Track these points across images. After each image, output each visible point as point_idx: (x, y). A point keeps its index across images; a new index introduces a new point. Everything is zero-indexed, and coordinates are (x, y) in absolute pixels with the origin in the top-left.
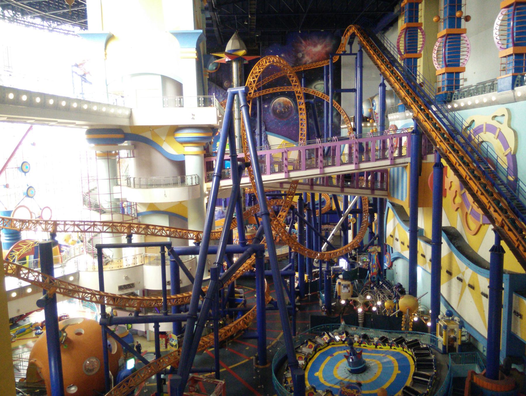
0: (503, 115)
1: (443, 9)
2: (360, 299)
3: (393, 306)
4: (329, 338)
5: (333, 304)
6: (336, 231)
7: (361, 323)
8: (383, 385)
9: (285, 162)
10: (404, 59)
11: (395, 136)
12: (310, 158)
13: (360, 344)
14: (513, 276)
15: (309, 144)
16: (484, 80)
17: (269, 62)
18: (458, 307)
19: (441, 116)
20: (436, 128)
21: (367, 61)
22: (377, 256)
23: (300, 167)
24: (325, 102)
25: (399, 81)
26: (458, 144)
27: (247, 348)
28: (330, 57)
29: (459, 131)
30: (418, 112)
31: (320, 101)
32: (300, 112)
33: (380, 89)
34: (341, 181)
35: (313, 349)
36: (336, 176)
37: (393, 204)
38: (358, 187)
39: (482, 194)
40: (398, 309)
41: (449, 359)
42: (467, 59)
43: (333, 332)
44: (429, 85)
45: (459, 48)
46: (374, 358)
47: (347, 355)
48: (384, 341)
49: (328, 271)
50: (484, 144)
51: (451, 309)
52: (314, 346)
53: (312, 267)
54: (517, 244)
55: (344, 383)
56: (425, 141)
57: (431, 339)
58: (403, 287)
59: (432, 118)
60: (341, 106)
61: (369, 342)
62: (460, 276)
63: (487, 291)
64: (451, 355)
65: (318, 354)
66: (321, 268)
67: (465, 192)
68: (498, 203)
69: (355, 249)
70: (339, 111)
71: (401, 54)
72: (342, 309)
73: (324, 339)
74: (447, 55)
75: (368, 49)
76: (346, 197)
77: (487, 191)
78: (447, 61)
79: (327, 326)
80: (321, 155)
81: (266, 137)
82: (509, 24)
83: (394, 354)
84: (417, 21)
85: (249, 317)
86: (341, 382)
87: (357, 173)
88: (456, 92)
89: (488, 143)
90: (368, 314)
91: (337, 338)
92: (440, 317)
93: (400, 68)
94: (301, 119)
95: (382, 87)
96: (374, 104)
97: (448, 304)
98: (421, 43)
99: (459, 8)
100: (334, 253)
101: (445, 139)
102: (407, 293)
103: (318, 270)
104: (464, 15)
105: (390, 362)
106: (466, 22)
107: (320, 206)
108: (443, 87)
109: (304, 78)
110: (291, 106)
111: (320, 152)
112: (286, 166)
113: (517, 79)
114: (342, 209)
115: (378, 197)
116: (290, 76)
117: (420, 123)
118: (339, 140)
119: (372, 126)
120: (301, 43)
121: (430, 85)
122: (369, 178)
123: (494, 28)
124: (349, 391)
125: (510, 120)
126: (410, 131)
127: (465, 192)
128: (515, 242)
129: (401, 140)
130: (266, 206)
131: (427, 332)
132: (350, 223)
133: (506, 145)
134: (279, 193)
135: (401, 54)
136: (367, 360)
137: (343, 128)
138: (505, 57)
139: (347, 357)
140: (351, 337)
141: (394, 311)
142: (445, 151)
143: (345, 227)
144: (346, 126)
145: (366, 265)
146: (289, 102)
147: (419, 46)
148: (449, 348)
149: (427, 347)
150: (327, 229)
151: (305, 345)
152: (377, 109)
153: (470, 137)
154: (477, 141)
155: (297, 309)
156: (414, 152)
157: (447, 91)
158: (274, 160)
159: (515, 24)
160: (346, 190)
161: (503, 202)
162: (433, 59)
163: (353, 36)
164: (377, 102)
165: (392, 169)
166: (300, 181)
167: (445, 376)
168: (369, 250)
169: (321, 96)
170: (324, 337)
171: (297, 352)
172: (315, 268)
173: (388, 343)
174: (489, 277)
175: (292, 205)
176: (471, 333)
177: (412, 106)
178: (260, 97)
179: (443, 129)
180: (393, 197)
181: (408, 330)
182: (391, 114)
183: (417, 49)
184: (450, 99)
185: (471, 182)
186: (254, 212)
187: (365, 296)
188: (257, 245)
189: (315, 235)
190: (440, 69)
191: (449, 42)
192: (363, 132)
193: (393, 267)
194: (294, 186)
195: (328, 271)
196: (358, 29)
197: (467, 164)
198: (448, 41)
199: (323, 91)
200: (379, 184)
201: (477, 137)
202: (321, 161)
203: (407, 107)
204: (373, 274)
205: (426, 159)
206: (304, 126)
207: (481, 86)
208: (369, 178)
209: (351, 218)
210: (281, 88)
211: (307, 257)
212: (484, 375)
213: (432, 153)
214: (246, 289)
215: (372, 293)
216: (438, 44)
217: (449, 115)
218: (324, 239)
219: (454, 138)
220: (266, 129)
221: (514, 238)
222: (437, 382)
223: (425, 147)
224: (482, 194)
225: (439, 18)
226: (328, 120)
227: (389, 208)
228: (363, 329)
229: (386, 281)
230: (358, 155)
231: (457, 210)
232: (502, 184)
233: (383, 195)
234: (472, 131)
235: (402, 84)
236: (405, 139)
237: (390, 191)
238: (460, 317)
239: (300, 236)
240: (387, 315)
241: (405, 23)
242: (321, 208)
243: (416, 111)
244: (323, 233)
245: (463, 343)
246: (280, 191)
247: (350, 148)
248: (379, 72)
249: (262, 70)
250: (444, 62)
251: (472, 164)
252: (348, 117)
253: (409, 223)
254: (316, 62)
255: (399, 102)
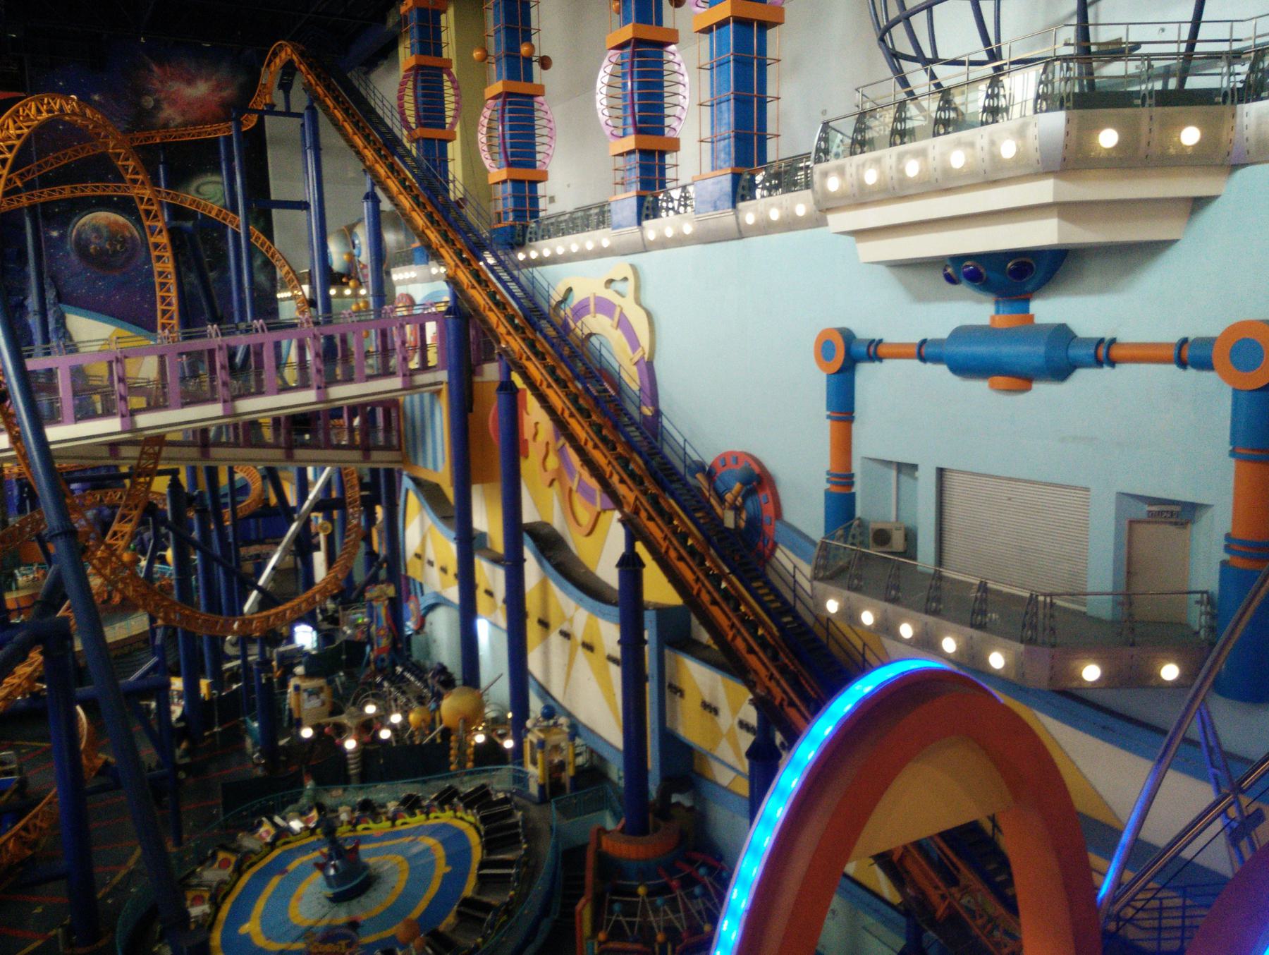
0: (625, 279)
1: (492, 34)
2: (351, 716)
3: (428, 719)
4: (273, 831)
5: (282, 742)
6: (281, 560)
7: (355, 775)
8: (409, 911)
9: (118, 387)
10: (417, 141)
11: (410, 319)
12: (195, 375)
13: (355, 825)
14: (663, 612)
15: (188, 337)
16: (587, 202)
17: (49, 111)
18: (565, 693)
19: (505, 277)
20: (497, 304)
21: (329, 135)
22: (386, 607)
23: (165, 400)
24: (230, 231)
25: (408, 189)
26: (543, 341)
27: (39, 910)
28: (234, 115)
29: (542, 310)
30: (457, 266)
31: (213, 229)
32: (157, 253)
33: (366, 207)
34: (283, 431)
35: (231, 868)
36: (269, 421)
37: (417, 482)
38: (329, 446)
39: (596, 446)
40: (441, 722)
41: (552, 811)
42: (550, 152)
43: (283, 814)
44: (475, 204)
45: (532, 128)
46: (389, 850)
47: (322, 860)
48: (411, 804)
49: (265, 663)
50: (593, 339)
51: (551, 703)
52: (233, 859)
53: (221, 657)
54: (664, 545)
55: (314, 934)
56: (477, 332)
57: (514, 777)
58: (450, 669)
59: (486, 281)
60: (272, 242)
61: (375, 817)
62: (565, 627)
63: (616, 651)
64: (556, 802)
65: (246, 878)
66: (244, 656)
67: (563, 446)
68: (625, 462)
69: (334, 598)
70: (269, 256)
71: (409, 128)
72: (306, 750)
73: (260, 835)
74: (508, 141)
75: (328, 107)
76: (302, 473)
77: (604, 440)
78: (509, 153)
79: (268, 801)
80: (223, 367)
81: (61, 321)
82: (625, 85)
83: (434, 831)
84: (438, 53)
85: (35, 825)
86: (307, 933)
87: (325, 411)
88: (533, 225)
89: (599, 337)
90: (371, 746)
91: (296, 825)
92: (529, 724)
93: (408, 160)
94: (161, 274)
95: (370, 203)
96: (357, 242)
97: (545, 693)
98: (453, 106)
99: (527, 37)
100: (276, 614)
101: (516, 328)
102: (459, 682)
103: (238, 662)
104: (537, 54)
105: (428, 851)
106: (543, 71)
107: (233, 499)
108: (506, 213)
109: (164, 163)
110: (132, 237)
111: (220, 359)
112: (123, 398)
113: (646, 204)
114: (292, 500)
115: (382, 466)
116: (118, 155)
117: (462, 291)
118: (269, 329)
119: (355, 295)
120: (151, 71)
121: (478, 204)
122: (356, 422)
123: (598, 91)
124: (328, 948)
125: (638, 288)
126: (443, 309)
127: (563, 446)
128: (661, 541)
129: (423, 329)
130: (63, 511)
131: (506, 763)
132: (317, 534)
133: (634, 343)
134: (113, 472)
135: (409, 128)
136: (371, 861)
137: (283, 300)
138: (621, 155)
139: (322, 867)
140: (330, 815)
141: (432, 730)
142: (517, 356)
143: (304, 545)
144: (288, 294)
145: (363, 632)
146: (124, 226)
147: (449, 113)
148: (553, 787)
149: (506, 797)
150: (258, 556)
151: (208, 863)
152: (365, 256)
153: (565, 325)
154: (579, 333)
155: (182, 775)
156: (453, 360)
157: (515, 220)
158: (91, 383)
159: (636, 86)
160: (299, 453)
161: (635, 462)
162: (480, 145)
163: (289, 69)
164: (362, 237)
165: (408, 398)
166: (169, 437)
167: (547, 850)
168: (368, 595)
169: (217, 215)
170: (262, 830)
171: (190, 887)
172: (230, 659)
173: (421, 807)
174: (617, 619)
175: (150, 503)
176: (593, 746)
177: (442, 251)
178: (32, 208)
179: (510, 305)
180: (416, 464)
181: (464, 767)
182: (398, 269)
183: (443, 118)
184: (521, 239)
185: (573, 422)
186: (32, 530)
187: (362, 709)
188: (47, 620)
189: (226, 573)
190: (496, 172)
191: (510, 111)
192: (335, 309)
193: (427, 629)
194: (151, 451)
195: (265, 663)
196: (302, 55)
197: (562, 384)
198: (507, 107)
199: (222, 202)
200: (381, 437)
201: (579, 324)
202: (225, 384)
203: (432, 254)
204: (381, 650)
205: (481, 374)
206: (168, 290)
207: (580, 214)
208: (356, 422)
209: (320, 521)
210: (98, 187)
211: (203, 632)
212: (622, 831)
213: (492, 360)
214: (24, 747)
215: (378, 697)
216: (487, 113)
217: (522, 275)
218: (248, 583)
219: (535, 327)
220: (60, 298)
221: (658, 535)
222: (529, 866)
223: (478, 345)
224: (596, 446)
225: (485, 51)
226: (241, 279)
227: (407, 491)
228: (361, 788)
229: (413, 664)
230: (322, 367)
231: (551, 484)
232: (632, 424)
233: (391, 462)
234: (568, 311)
235: (416, 199)
236: (431, 328)
237: (407, 448)
238: (569, 715)
239: (179, 581)
240: (417, 742)
241: (412, 53)
242: (234, 504)
243: (453, 264)
244: (249, 567)
245: (580, 771)
246: (116, 467)
247: (301, 349)
248: (362, 167)
249: (26, 131)
250: (502, 155)
251: (573, 383)
252: (294, 272)
253: (455, 521)
254: (195, 124)
255: (414, 242)
